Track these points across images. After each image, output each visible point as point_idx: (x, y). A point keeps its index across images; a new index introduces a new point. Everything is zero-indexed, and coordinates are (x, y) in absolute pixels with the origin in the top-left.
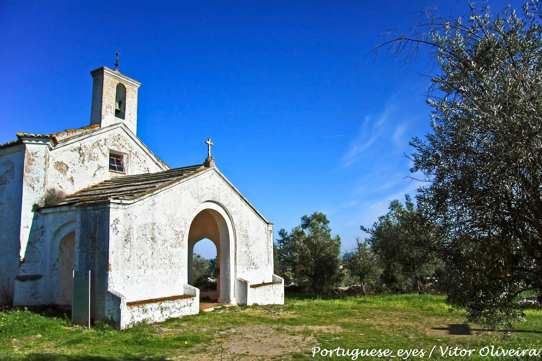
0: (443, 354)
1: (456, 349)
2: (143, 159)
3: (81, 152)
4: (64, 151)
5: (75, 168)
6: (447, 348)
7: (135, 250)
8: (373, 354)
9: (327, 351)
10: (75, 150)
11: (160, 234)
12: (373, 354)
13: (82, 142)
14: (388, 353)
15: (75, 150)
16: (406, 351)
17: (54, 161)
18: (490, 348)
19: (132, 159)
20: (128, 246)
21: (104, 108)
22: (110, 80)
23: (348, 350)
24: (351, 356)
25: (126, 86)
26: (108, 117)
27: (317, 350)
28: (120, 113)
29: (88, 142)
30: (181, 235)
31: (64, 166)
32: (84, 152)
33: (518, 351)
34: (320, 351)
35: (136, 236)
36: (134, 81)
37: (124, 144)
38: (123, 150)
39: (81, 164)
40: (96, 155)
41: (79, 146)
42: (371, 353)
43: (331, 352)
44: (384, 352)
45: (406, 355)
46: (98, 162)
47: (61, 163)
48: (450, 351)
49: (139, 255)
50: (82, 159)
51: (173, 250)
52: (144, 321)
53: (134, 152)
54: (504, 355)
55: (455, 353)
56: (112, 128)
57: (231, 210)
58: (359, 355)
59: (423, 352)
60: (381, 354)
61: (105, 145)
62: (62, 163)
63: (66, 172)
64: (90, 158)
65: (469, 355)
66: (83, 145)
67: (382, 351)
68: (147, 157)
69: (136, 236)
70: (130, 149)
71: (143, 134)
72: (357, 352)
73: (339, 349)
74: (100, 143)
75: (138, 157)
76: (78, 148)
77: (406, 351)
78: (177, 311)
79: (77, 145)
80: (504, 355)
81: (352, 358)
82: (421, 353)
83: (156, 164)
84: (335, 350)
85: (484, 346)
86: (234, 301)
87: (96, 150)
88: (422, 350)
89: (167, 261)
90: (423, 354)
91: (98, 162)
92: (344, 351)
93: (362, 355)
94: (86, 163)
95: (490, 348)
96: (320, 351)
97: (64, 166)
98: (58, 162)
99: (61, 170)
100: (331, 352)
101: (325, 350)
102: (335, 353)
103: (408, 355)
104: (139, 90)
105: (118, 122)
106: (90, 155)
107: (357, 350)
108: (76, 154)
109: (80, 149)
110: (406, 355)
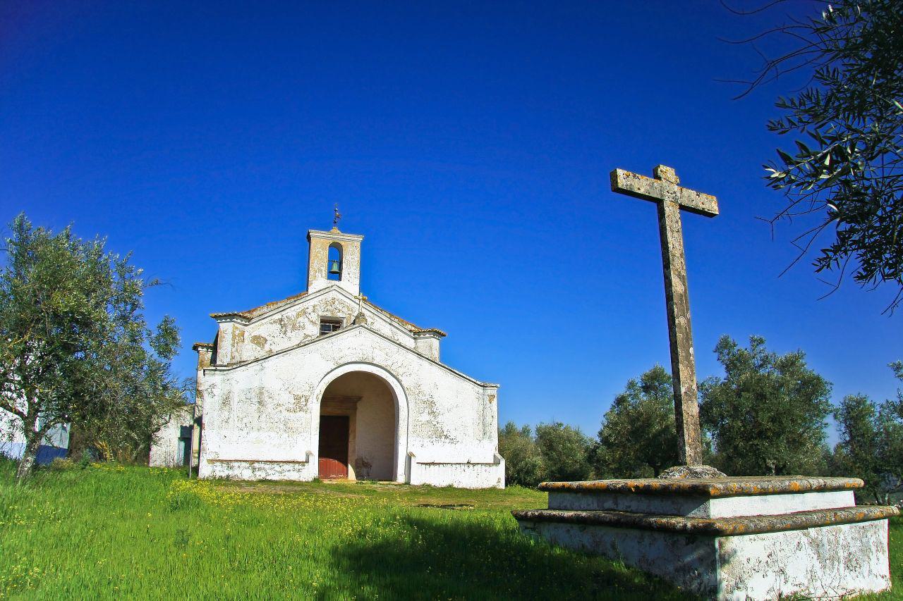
3: (283, 323)
5: (276, 340)
7: (235, 413)
10: (275, 322)
11: (270, 398)
13: (283, 313)
20: (227, 408)
21: (311, 272)
22: (320, 244)
25: (342, 243)
26: (318, 281)
28: (335, 275)
29: (291, 312)
30: (303, 399)
35: (236, 400)
38: (340, 315)
39: (282, 335)
40: (302, 324)
46: (305, 331)
49: (241, 416)
51: (288, 414)
52: (228, 476)
56: (322, 292)
57: (393, 369)
61: (314, 312)
63: (263, 345)
64: (294, 328)
69: (236, 400)
70: (350, 312)
78: (277, 474)
79: (278, 316)
83: (390, 324)
86: (401, 478)
87: (301, 319)
89: (282, 426)
91: (305, 331)
94: (289, 334)
99: (258, 344)
104: (363, 245)
105: (330, 285)
109: (281, 320)
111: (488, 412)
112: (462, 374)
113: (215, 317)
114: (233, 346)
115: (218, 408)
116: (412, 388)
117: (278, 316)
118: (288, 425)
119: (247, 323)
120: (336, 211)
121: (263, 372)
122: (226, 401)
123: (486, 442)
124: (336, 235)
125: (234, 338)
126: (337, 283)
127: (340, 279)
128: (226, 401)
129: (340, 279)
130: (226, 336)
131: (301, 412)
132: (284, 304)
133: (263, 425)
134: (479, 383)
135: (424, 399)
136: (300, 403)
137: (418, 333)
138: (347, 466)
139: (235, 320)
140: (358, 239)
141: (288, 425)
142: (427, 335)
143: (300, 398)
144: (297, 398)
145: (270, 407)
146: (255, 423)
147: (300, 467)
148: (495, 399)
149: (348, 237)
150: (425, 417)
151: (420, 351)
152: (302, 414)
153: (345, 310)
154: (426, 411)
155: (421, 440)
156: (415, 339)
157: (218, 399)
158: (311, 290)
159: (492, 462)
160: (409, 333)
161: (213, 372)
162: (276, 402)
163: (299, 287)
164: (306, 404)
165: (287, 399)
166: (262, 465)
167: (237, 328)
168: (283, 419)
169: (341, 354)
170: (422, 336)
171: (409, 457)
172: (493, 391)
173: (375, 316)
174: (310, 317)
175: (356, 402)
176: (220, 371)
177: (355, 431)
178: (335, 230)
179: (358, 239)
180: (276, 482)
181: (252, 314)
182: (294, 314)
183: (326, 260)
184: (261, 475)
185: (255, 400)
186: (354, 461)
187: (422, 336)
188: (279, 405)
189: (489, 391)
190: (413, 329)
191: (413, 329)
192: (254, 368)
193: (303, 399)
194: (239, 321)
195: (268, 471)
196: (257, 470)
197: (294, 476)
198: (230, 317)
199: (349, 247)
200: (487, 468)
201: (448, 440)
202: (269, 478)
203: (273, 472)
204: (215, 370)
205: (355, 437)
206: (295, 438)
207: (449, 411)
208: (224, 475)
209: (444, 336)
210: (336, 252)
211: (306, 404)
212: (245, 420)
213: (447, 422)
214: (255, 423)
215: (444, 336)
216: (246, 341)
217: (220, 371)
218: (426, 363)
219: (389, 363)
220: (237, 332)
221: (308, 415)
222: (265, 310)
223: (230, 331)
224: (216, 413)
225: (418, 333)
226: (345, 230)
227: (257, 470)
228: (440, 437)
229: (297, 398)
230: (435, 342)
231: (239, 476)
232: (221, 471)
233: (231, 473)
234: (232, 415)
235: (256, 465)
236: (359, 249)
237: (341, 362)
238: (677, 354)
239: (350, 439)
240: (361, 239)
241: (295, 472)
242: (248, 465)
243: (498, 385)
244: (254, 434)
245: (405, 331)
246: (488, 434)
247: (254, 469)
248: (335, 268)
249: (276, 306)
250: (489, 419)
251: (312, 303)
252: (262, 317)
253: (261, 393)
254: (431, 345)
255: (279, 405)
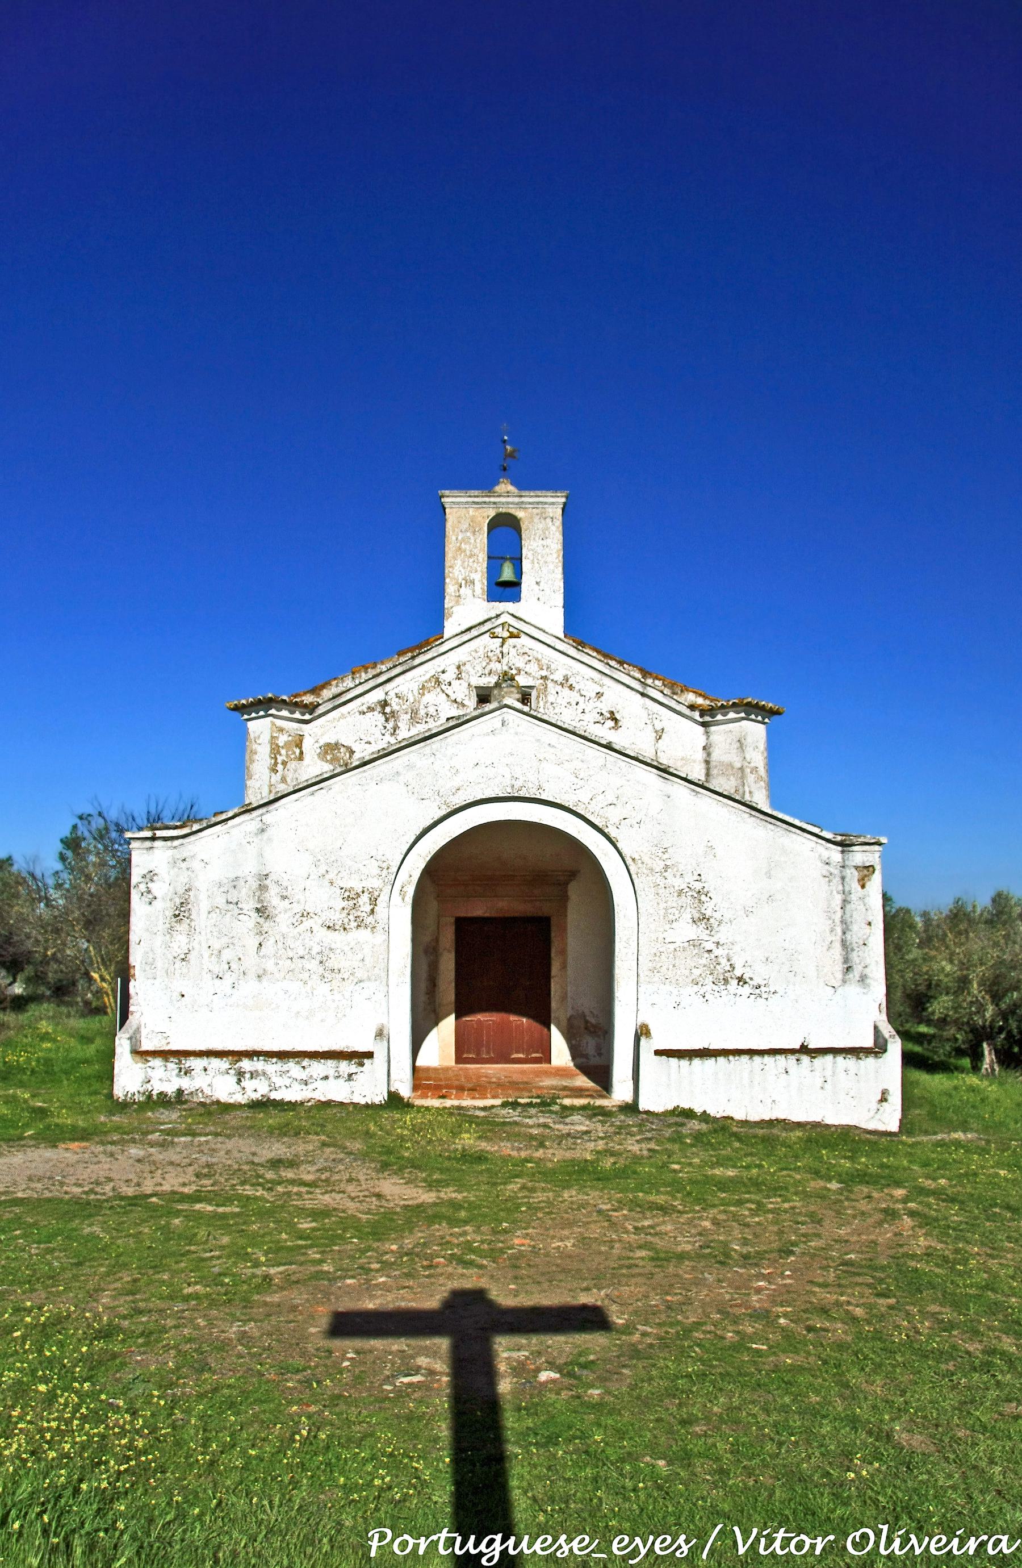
0: (742, 1550)
1: (781, 1534)
2: (591, 689)
3: (388, 710)
4: (343, 716)
6: (755, 1531)
8: (542, 1549)
9: (411, 1542)
10: (371, 709)
11: (284, 898)
12: (542, 1549)
13: (388, 687)
14: (587, 1547)
15: (371, 709)
16: (638, 1540)
17: (318, 745)
18: (878, 1534)
19: (551, 698)
20: (184, 927)
21: (450, 588)
22: (466, 522)
23: (473, 1538)
24: (481, 1554)
25: (520, 514)
26: (466, 604)
27: (382, 1537)
28: (505, 589)
29: (407, 684)
30: (365, 898)
31: (342, 750)
32: (396, 707)
33: (955, 1542)
34: (393, 1540)
35: (204, 905)
36: (539, 493)
37: (521, 665)
40: (432, 710)
41: (382, 697)
42: (537, 1546)
43: (423, 1544)
44: (575, 1544)
45: (636, 1552)
47: (336, 746)
48: (763, 1540)
49: (216, 945)
50: (391, 725)
52: (180, 1092)
53: (558, 677)
54: (918, 1551)
55: (777, 1544)
56: (474, 633)
58: (504, 1553)
59: (687, 1542)
60: (566, 1548)
62: (336, 744)
65: (421, 1552)
66: (392, 694)
67: (569, 1540)
68: (607, 681)
70: (544, 673)
71: (582, 627)
72: (497, 1545)
73: (444, 1534)
74: (442, 677)
75: (571, 687)
76: (379, 702)
77: (638, 1540)
78: (296, 1086)
79: (378, 695)
80: (918, 1551)
81: (484, 1561)
82: (560, 1547)
83: (643, 694)
84: (434, 1537)
85: (863, 1525)
86: (621, 1092)
87: (429, 698)
88: (683, 1537)
89: (313, 965)
90: (685, 1548)
92: (459, 1539)
93: (511, 1552)
95: (878, 1534)
96: (393, 1540)
97: (342, 750)
98: (328, 745)
100: (423, 1544)
101: (406, 1537)
102: (434, 1544)
103: (643, 1552)
106: (414, 713)
107: (498, 1537)
108: (375, 718)
109: (384, 704)
110: (636, 1552)
111: (857, 914)
112: (780, 816)
113: (236, 708)
114: (274, 770)
115: (162, 927)
116: (646, 859)
117: (378, 695)
118: (330, 964)
119: (307, 717)
120: (505, 441)
121: (265, 835)
122: (181, 913)
123: (853, 990)
124: (506, 496)
125: (275, 750)
126: (509, 606)
127: (516, 598)
128: (181, 913)
129: (516, 598)
130: (259, 748)
131: (361, 930)
132: (390, 665)
133: (270, 965)
134: (829, 835)
135: (679, 883)
136: (358, 908)
137: (711, 711)
138: (549, 1029)
139: (273, 711)
140: (554, 503)
141: (330, 964)
142: (732, 715)
143: (358, 895)
144: (351, 896)
145: (283, 921)
146: (251, 961)
147: (353, 1068)
148: (877, 879)
149: (530, 497)
150: (686, 931)
151: (664, 760)
152: (364, 934)
153: (532, 668)
154: (687, 916)
155: (675, 992)
156: (704, 724)
157: (163, 907)
158: (450, 627)
159: (869, 1042)
160: (687, 712)
161: (148, 844)
162: (297, 908)
163: (420, 627)
164: (372, 911)
165: (325, 901)
166: (259, 1065)
167: (281, 730)
168: (316, 949)
169: (457, 782)
170: (719, 717)
171: (642, 1032)
172: (871, 856)
173: (604, 678)
174: (449, 692)
175: (566, 884)
176: (165, 839)
177: (563, 952)
178: (505, 487)
179: (554, 503)
180: (292, 1106)
181: (319, 695)
182: (415, 687)
183: (483, 557)
184: (255, 1089)
185: (249, 905)
186: (564, 1023)
187: (719, 717)
188: (305, 915)
189: (860, 856)
190: (700, 701)
191: (700, 701)
192: (243, 827)
193: (365, 898)
194: (285, 713)
195: (274, 1079)
196: (248, 1076)
197: (337, 1091)
198: (264, 705)
199: (536, 520)
200: (851, 1062)
201: (746, 990)
202: (275, 1096)
203: (288, 1082)
204: (153, 839)
205: (564, 967)
206: (347, 995)
207: (748, 913)
208: (170, 1089)
209: (777, 713)
210: (505, 536)
211: (372, 911)
212: (227, 955)
213: (743, 944)
214: (251, 961)
215: (777, 713)
216: (307, 757)
217: (165, 839)
218: (681, 789)
219: (584, 796)
220: (283, 739)
221: (380, 937)
222: (349, 683)
223: (265, 738)
224: (159, 940)
225: (711, 711)
226: (524, 484)
227: (248, 1076)
228: (726, 981)
229: (351, 896)
230: (755, 732)
231: (207, 1091)
232: (165, 1080)
233: (186, 1084)
234: (195, 944)
235: (246, 1064)
236: (559, 522)
237: (459, 801)
238: (498, 1460)
239: (555, 970)
240: (564, 500)
241: (341, 1081)
242: (227, 1066)
243: (884, 840)
244: (249, 987)
245: (678, 707)
246: (857, 970)
247: (240, 1074)
248: (507, 573)
249: (371, 672)
250: (857, 932)
251: (454, 658)
252: (339, 702)
253: (263, 888)
254: (746, 739)
255: (305, 915)
